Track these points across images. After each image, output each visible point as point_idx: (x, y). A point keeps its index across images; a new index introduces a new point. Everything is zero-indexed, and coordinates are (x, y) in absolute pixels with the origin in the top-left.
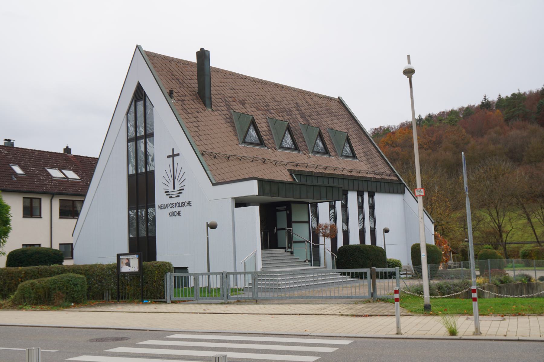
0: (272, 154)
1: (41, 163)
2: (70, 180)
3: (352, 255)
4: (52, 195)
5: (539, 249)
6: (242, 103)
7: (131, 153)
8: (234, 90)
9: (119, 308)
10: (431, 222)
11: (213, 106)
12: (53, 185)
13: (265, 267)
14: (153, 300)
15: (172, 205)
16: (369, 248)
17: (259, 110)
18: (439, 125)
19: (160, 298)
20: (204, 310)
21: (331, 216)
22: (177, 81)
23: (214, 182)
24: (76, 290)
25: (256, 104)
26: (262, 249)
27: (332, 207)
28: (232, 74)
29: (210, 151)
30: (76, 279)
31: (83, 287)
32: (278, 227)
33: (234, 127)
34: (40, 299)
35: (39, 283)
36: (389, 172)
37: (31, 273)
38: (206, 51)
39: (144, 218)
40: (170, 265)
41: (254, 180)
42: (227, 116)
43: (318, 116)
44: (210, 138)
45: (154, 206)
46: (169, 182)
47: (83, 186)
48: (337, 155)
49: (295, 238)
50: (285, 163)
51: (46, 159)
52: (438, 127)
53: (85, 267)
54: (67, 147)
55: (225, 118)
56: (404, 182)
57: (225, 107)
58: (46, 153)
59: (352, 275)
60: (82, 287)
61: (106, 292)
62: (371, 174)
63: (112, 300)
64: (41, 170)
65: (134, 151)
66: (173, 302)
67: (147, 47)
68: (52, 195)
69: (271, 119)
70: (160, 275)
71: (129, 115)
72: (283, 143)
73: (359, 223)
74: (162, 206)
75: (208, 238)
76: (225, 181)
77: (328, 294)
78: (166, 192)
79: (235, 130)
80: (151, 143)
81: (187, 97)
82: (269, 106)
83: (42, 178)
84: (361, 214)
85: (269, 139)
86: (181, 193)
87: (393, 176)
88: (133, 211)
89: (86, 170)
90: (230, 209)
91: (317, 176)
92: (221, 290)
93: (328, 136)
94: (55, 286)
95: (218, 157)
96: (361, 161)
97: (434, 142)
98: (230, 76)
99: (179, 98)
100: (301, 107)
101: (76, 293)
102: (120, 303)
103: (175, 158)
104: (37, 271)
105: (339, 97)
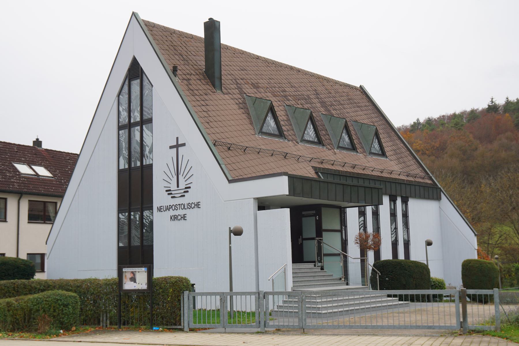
0: (293, 148)
1: (7, 156)
2: (41, 177)
3: (391, 272)
4: (20, 194)
6: (256, 86)
7: (123, 143)
8: (245, 71)
9: (125, 337)
10: (473, 234)
11: (223, 88)
12: (22, 183)
13: (296, 285)
14: (165, 327)
15: (175, 207)
16: (411, 264)
17: (275, 96)
18: (442, 128)
20: (244, 342)
21: (360, 224)
22: (181, 57)
23: (230, 179)
24: (66, 313)
25: (271, 89)
26: (293, 262)
27: (362, 214)
28: (243, 53)
29: (223, 140)
30: (66, 298)
31: (76, 309)
32: (304, 237)
33: (249, 114)
34: (18, 324)
35: (17, 303)
36: (423, 174)
37: (4, 290)
38: (215, 22)
39: (137, 222)
40: (188, 282)
41: (284, 176)
42: (239, 100)
43: (340, 106)
44: (222, 125)
45: (151, 208)
47: (56, 186)
48: (365, 152)
49: (326, 249)
50: (309, 159)
51: (12, 153)
52: (441, 131)
53: (76, 282)
54: (37, 139)
55: (238, 103)
56: (440, 186)
57: (237, 90)
58: (13, 146)
59: (401, 298)
60: (74, 308)
62: (404, 175)
63: (110, 326)
64: (7, 165)
65: (127, 140)
66: (192, 330)
67: (143, 16)
68: (20, 195)
69: (289, 107)
70: (175, 294)
71: (120, 96)
72: (305, 135)
73: (392, 234)
75: (230, 248)
76: (247, 177)
77: (391, 322)
78: (167, 191)
79: (249, 118)
81: (192, 76)
82: (285, 91)
83: (8, 174)
84: (393, 223)
85: (288, 130)
86: (187, 192)
87: (428, 179)
88: (123, 214)
89: (59, 166)
90: (252, 213)
91: (352, 177)
92: (257, 315)
93: (353, 129)
94: (39, 307)
95: (233, 149)
96: (391, 160)
97: (437, 148)
98: (240, 54)
99: (184, 76)
100: (321, 95)
101: (66, 317)
102: (122, 330)
103: (180, 148)
104: (12, 286)
105: (360, 86)
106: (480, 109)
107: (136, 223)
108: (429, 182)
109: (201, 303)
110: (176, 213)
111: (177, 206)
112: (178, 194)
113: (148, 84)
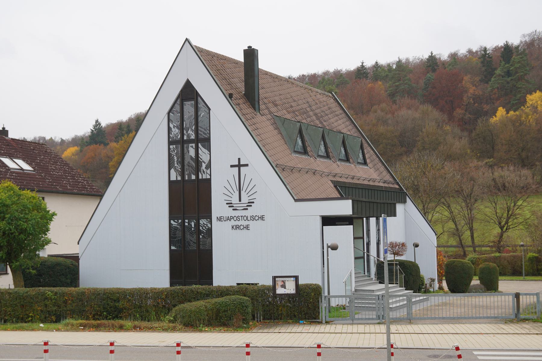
2: (25, 171)
5: (486, 257)
10: (434, 234)
15: (238, 218)
19: (315, 319)
27: (378, 219)
36: (391, 180)
38: (255, 50)
39: (193, 229)
45: (209, 217)
46: (247, 192)
61: (257, 314)
63: (263, 321)
66: (327, 323)
71: (171, 114)
74: (222, 218)
78: (227, 204)
80: (205, 149)
86: (251, 206)
106: (344, 70)
107: (191, 229)
108: (397, 187)
109: (334, 303)
110: (237, 223)
111: (239, 217)
112: (240, 208)
113: (205, 107)
